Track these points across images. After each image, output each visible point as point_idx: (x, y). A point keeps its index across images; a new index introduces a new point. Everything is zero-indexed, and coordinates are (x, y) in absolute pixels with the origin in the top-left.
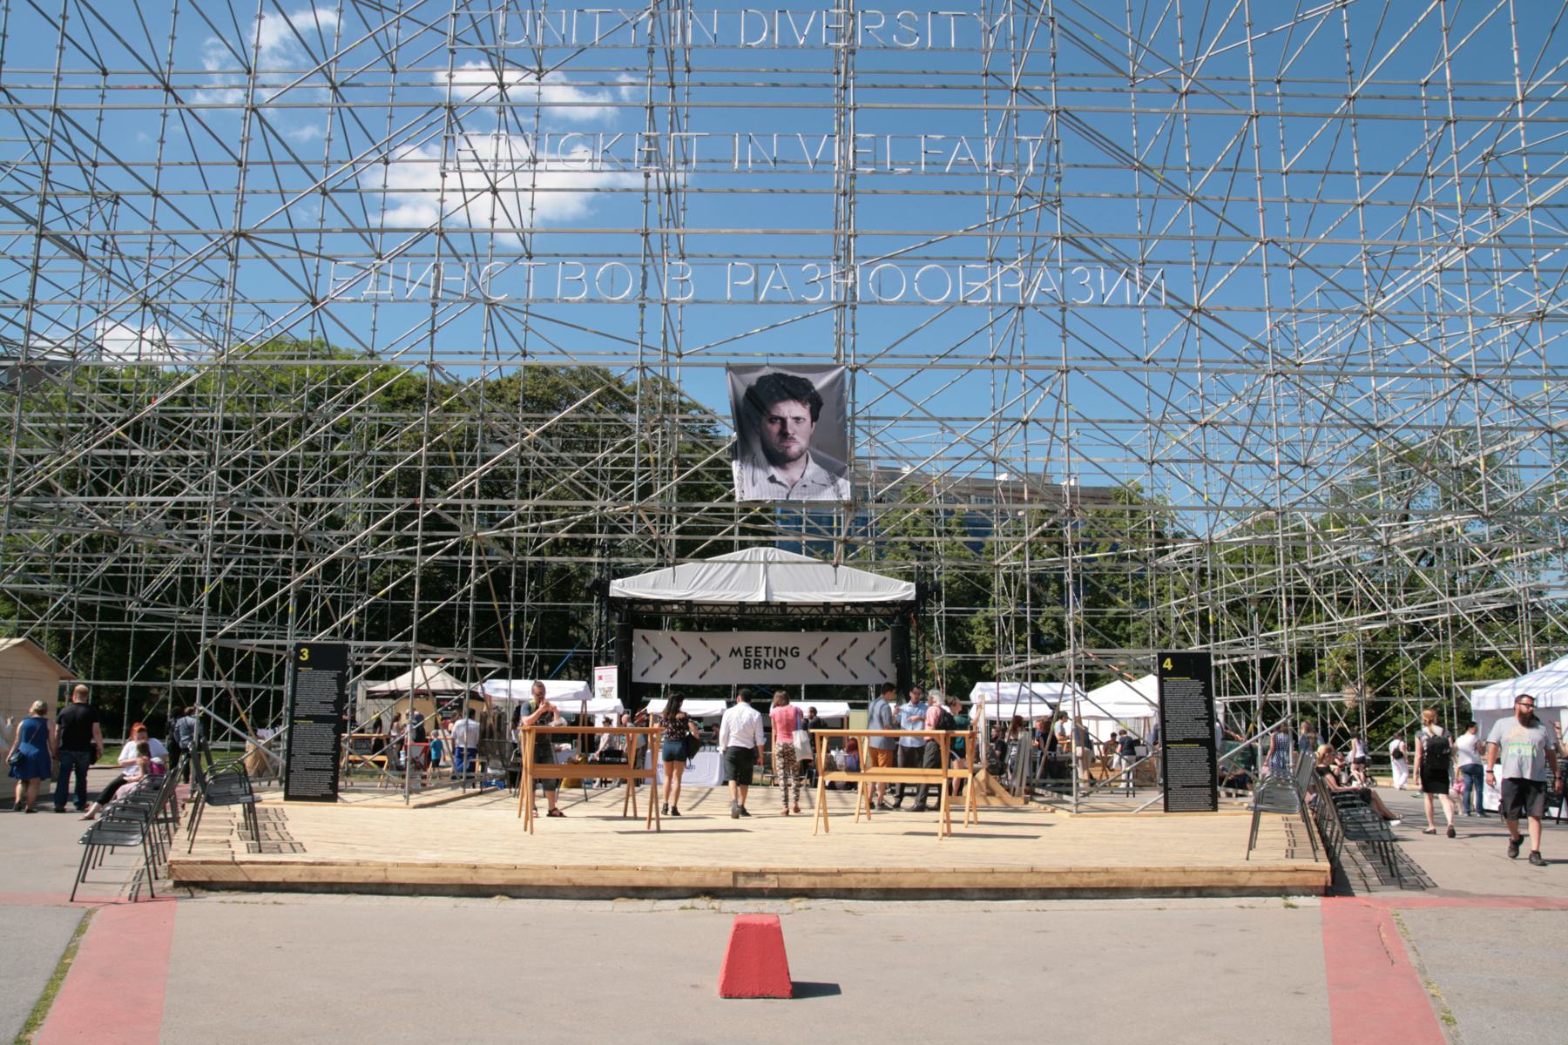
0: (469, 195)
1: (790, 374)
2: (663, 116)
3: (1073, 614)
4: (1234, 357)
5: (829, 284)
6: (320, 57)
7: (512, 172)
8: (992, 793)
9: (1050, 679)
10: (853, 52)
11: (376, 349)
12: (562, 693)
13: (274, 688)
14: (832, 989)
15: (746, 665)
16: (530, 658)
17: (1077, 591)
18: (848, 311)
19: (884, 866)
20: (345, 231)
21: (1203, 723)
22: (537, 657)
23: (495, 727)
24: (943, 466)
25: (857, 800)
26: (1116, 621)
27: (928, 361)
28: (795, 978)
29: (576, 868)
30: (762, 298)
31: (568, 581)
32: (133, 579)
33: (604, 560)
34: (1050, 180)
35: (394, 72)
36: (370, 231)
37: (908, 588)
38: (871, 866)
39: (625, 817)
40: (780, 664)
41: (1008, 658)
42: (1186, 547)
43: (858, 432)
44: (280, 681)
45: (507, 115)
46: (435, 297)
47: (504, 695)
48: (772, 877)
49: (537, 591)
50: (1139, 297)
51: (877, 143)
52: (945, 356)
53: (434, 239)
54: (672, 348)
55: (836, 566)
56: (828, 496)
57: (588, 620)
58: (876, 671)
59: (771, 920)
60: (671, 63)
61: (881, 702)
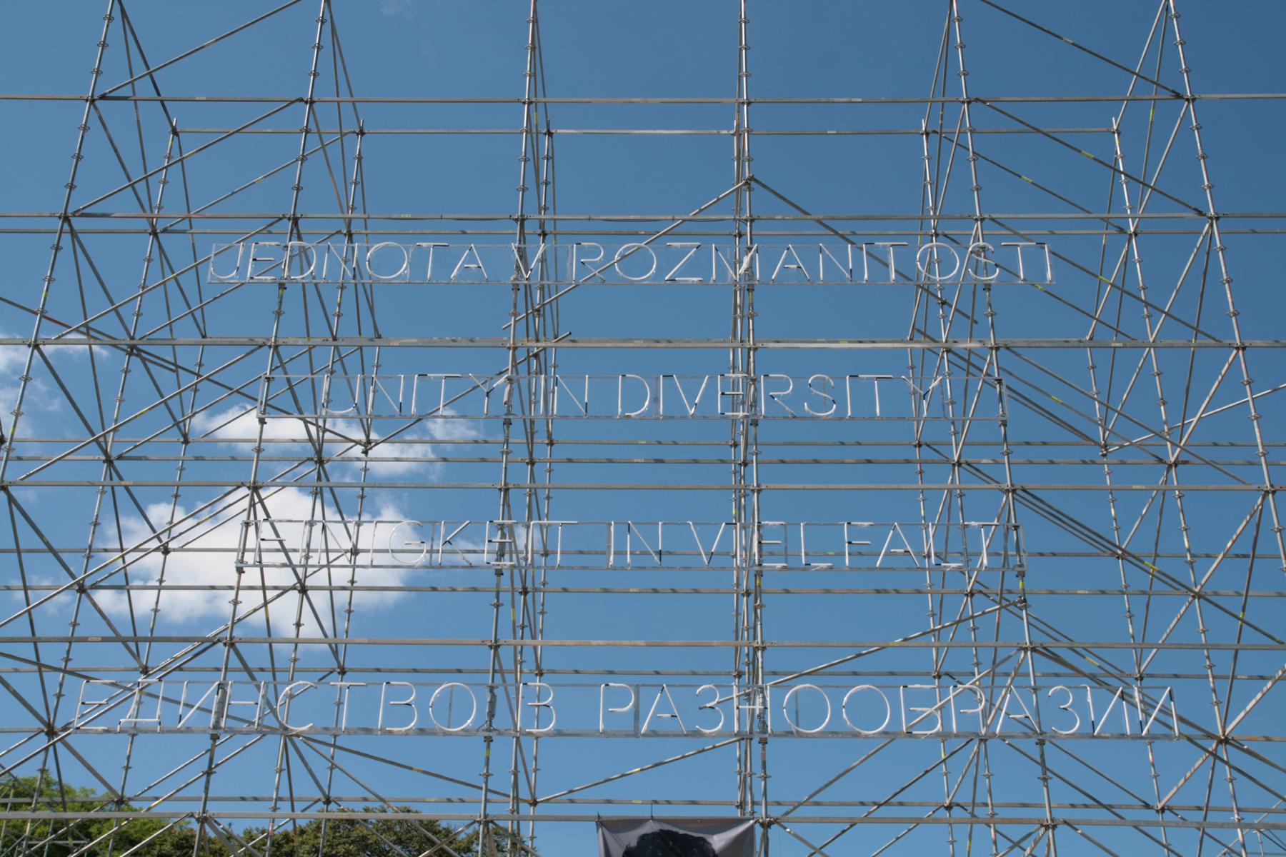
0: (271, 594)
2: (520, 499)
5: (727, 710)
10: (755, 423)
11: (128, 794)
20: (105, 640)
27: (862, 812)
30: (644, 729)
34: (1010, 575)
35: (186, 442)
36: (137, 640)
46: (217, 726)
51: (788, 531)
52: (886, 803)
54: (524, 793)
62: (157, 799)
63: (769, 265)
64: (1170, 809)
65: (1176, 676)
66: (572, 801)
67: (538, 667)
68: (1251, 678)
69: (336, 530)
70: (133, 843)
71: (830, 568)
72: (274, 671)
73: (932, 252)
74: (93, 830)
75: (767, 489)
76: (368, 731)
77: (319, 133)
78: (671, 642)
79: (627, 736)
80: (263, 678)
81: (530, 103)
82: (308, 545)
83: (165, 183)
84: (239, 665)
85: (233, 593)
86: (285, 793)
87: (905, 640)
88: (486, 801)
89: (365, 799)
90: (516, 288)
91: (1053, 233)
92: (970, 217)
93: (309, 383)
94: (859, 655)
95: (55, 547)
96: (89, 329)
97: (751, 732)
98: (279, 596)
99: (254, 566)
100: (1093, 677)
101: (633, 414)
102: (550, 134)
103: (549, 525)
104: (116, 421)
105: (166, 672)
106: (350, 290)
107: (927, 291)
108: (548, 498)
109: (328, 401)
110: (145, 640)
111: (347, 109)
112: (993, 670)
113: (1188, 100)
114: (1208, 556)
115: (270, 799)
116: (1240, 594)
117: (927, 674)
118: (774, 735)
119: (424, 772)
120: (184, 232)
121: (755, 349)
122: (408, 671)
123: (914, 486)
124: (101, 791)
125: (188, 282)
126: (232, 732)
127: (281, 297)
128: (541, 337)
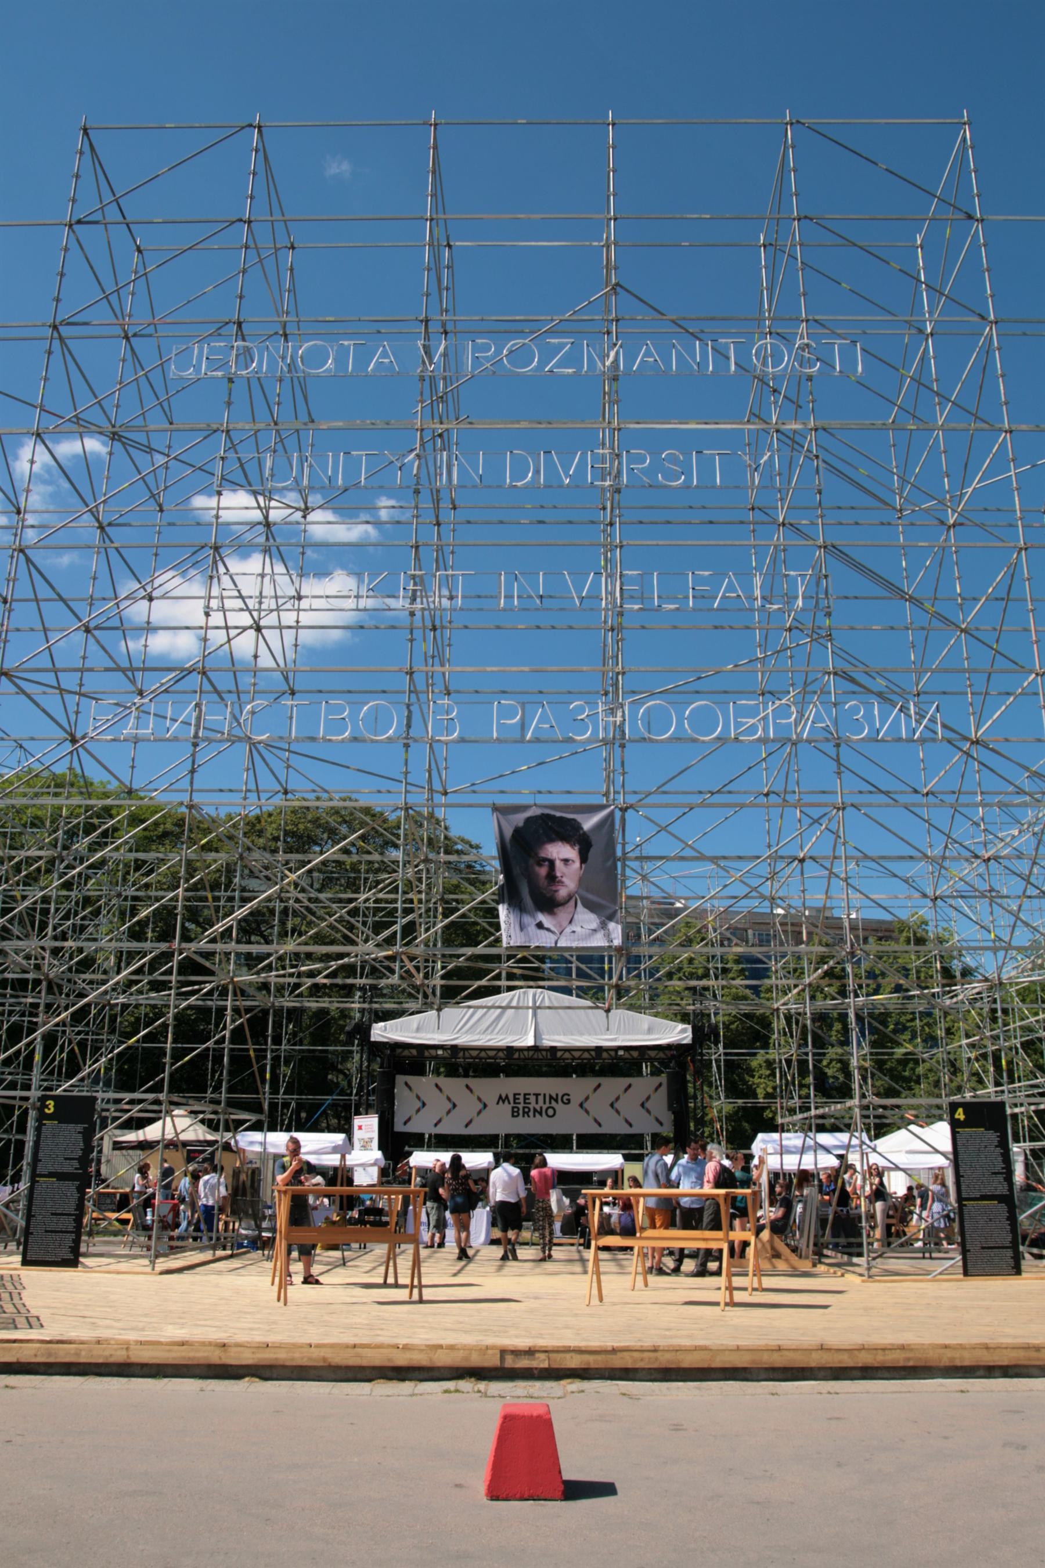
0: (233, 633)
1: (558, 814)
2: (429, 555)
3: (858, 1055)
5: (595, 721)
6: (89, 498)
7: (278, 610)
8: (777, 1255)
9: (835, 1129)
10: (618, 491)
11: (135, 786)
12: (318, 1146)
13: (15, 1137)
14: (606, 1489)
16: (286, 1105)
17: (862, 1032)
18: (618, 750)
19: (662, 1343)
20: (107, 670)
21: (1001, 1178)
22: (293, 1104)
23: (248, 1184)
24: (720, 905)
25: (633, 1262)
26: (904, 1062)
27: (699, 799)
28: (567, 1476)
29: (332, 1346)
30: (529, 736)
31: (327, 1024)
33: (366, 1006)
34: (820, 615)
35: (161, 510)
36: (133, 670)
37: (683, 1031)
38: (648, 1343)
39: (385, 1285)
40: (551, 1112)
41: (791, 1103)
42: (977, 986)
43: (629, 872)
44: (22, 1129)
45: (270, 540)
46: (196, 736)
47: (258, 1148)
48: (542, 1356)
49: (294, 1034)
50: (914, 731)
51: (644, 579)
52: (718, 792)
53: (196, 679)
54: (437, 786)
55: (608, 1011)
56: (598, 941)
57: (349, 1065)
59: (541, 1411)
60: (437, 502)
61: (656, 1157)
62: (156, 790)
63: (630, 359)
64: (933, 794)
65: (944, 693)
66: (474, 792)
67: (446, 688)
68: (1000, 694)
69: (283, 581)
70: (143, 821)
71: (677, 609)
72: (238, 692)
73: (766, 348)
74: (114, 812)
75: (628, 545)
76: (313, 739)
77: (257, 248)
78: (550, 668)
79: (516, 742)
80: (230, 699)
81: (432, 220)
82: (261, 593)
83: (133, 294)
84: (210, 688)
85: (203, 631)
86: (253, 787)
87: (736, 666)
88: (407, 792)
89: (314, 791)
90: (422, 379)
91: (865, 333)
92: (797, 319)
93: (256, 460)
94: (699, 678)
95: (64, 596)
96: (78, 419)
97: (614, 738)
98: (239, 634)
99: (218, 610)
100: (880, 695)
101: (519, 484)
102: (449, 246)
103: (452, 575)
104: (105, 495)
105: (156, 694)
106: (287, 382)
107: (762, 380)
108: (452, 553)
109: (272, 476)
110: (138, 669)
111: (280, 227)
112: (804, 689)
113: (977, 220)
114: (974, 599)
115: (241, 791)
116: (995, 629)
117: (754, 692)
118: (631, 741)
119: (359, 770)
120: (150, 336)
121: (619, 430)
122: (343, 692)
123: (746, 543)
124: (114, 785)
125: (156, 378)
126: (210, 741)
127: (230, 390)
128: (445, 420)
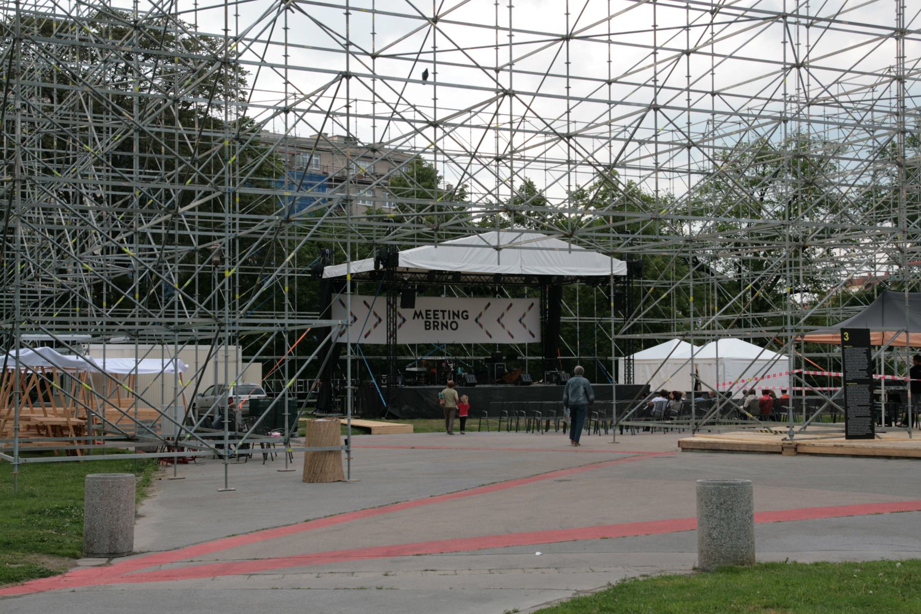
4: (811, 44)
15: (427, 327)
32: (290, 278)
40: (454, 326)
58: (526, 332)
